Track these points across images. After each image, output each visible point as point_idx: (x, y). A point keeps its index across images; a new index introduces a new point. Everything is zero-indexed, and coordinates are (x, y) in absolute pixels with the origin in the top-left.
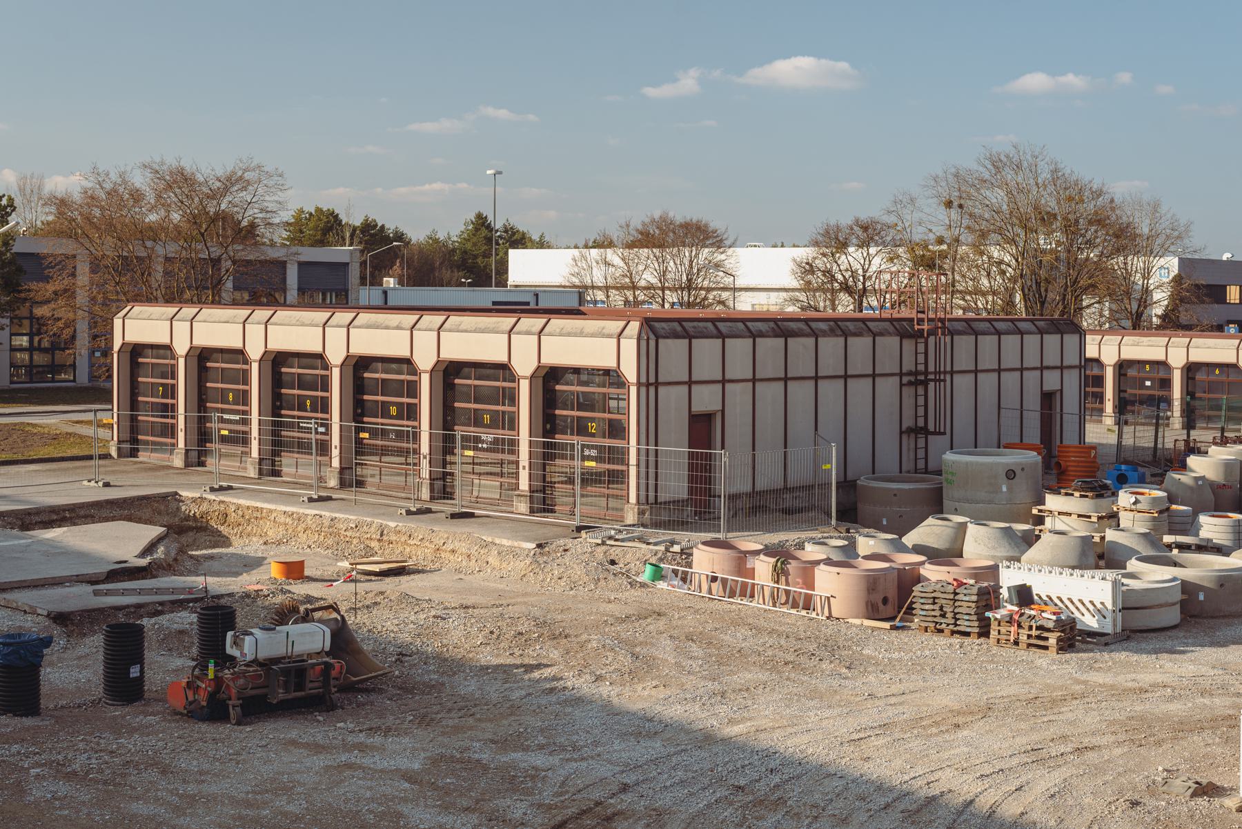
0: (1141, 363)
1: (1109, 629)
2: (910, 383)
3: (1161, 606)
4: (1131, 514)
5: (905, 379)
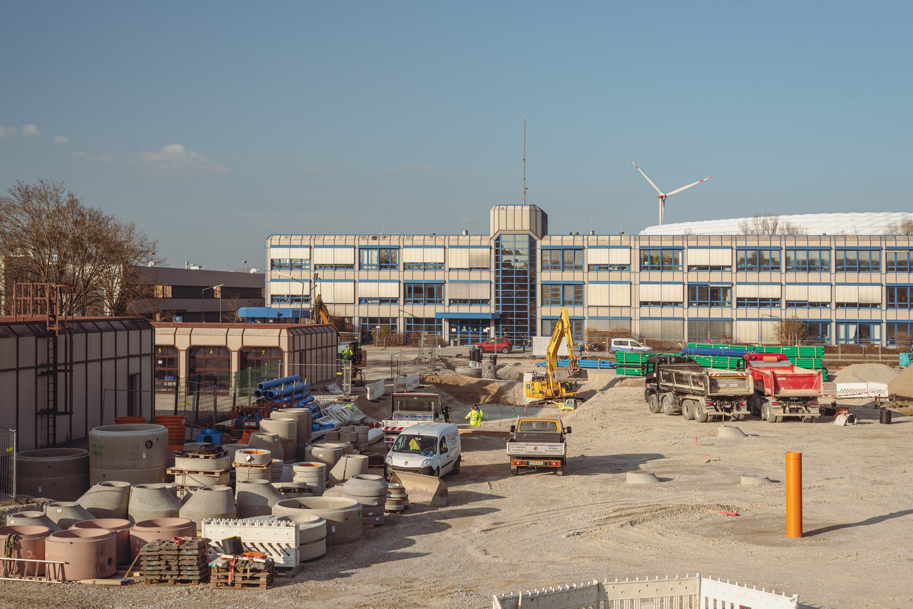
0: (206, 348)
1: (293, 564)
2: (43, 374)
3: (310, 543)
4: (246, 469)
5: (39, 371)
